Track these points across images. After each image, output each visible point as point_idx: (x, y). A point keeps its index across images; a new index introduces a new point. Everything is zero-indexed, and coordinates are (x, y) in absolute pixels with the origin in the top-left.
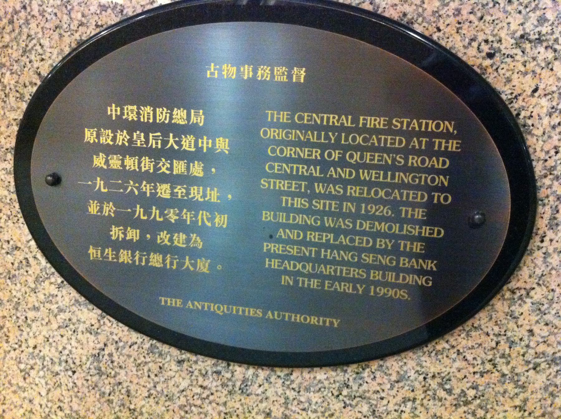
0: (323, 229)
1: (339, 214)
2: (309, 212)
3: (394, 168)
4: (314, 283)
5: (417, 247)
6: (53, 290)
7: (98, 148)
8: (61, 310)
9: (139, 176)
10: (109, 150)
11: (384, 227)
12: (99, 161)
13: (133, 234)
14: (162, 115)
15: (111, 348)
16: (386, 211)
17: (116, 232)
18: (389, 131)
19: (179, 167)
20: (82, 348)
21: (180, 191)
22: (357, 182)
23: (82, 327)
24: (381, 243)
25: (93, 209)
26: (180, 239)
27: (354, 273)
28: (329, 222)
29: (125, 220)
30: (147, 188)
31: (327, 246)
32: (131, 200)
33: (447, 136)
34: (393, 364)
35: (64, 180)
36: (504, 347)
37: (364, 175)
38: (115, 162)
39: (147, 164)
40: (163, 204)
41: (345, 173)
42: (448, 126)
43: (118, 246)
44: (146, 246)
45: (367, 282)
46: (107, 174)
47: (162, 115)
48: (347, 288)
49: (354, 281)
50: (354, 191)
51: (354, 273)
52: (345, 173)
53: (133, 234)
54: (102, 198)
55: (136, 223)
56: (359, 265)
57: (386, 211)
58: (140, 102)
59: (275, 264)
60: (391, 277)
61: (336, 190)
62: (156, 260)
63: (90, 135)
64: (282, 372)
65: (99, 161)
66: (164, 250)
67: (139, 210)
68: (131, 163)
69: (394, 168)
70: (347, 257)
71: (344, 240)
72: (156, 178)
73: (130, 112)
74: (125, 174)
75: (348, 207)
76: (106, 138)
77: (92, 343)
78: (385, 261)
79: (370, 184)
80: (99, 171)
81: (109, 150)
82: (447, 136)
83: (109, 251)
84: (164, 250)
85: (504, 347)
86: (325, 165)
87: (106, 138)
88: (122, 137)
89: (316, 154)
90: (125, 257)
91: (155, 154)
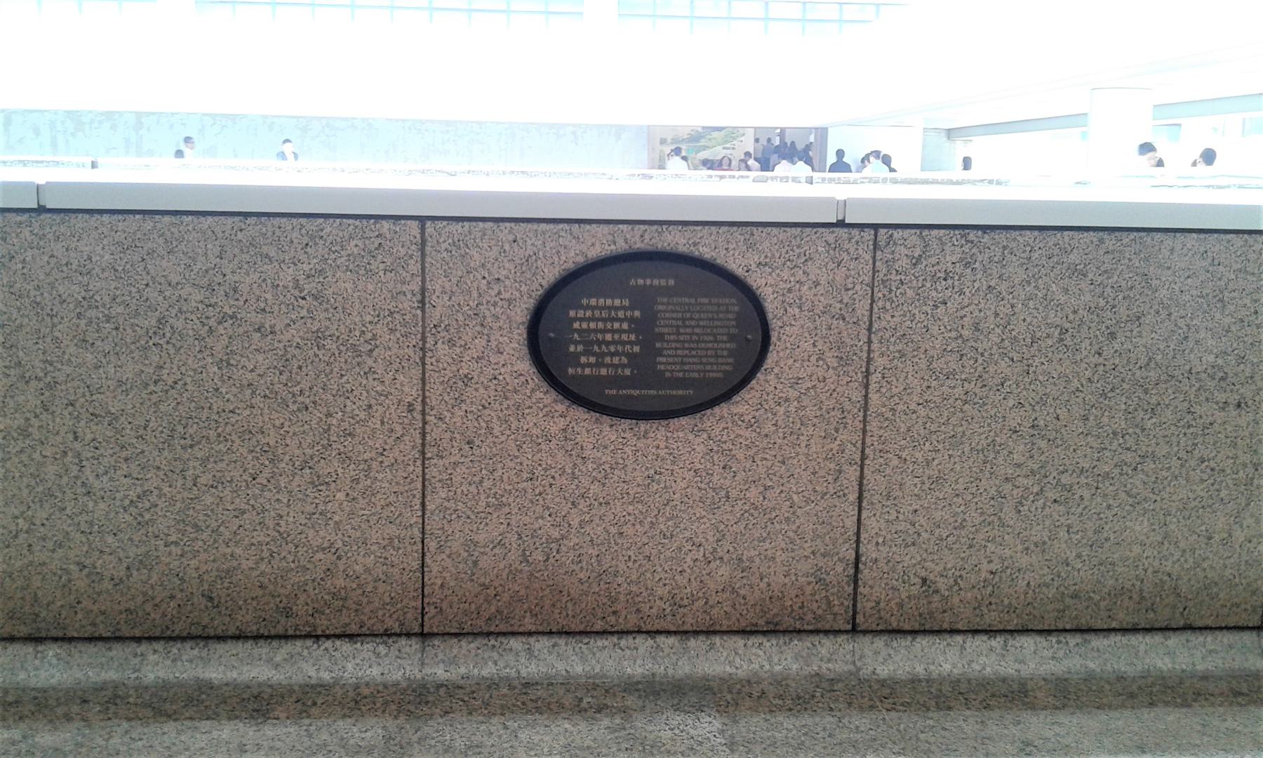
0: (684, 348)
1: (691, 341)
2: (678, 341)
3: (713, 319)
4: (681, 375)
5: (725, 353)
6: (542, 395)
7: (576, 319)
8: (545, 406)
9: (596, 331)
10: (581, 320)
11: (710, 345)
12: (576, 325)
13: (592, 360)
14: (609, 302)
15: (574, 423)
16: (711, 338)
17: (583, 360)
18: (710, 304)
19: (616, 325)
20: (556, 426)
21: (616, 337)
22: (698, 326)
23: (557, 414)
24: (709, 353)
25: (572, 349)
26: (616, 360)
27: (699, 367)
28: (687, 345)
29: (587, 353)
30: (600, 336)
31: (686, 356)
32: (591, 343)
33: (733, 305)
34: (717, 410)
35: (1136, 148)
36: (765, 396)
37: (701, 323)
38: (585, 326)
39: (601, 325)
40: (608, 344)
41: (693, 323)
42: (734, 301)
43: (583, 366)
44: (599, 365)
45: (705, 371)
46: (580, 331)
47: (609, 302)
48: (696, 375)
49: (698, 371)
50: (697, 330)
51: (699, 367)
52: (693, 323)
53: (592, 360)
54: (576, 343)
55: (594, 354)
56: (701, 363)
57: (711, 338)
58: (605, 297)
59: (662, 367)
60: (715, 367)
61: (689, 330)
62: (604, 372)
63: (572, 313)
64: (664, 422)
65: (576, 325)
66: (608, 366)
67: (596, 348)
68: (592, 325)
69: (713, 319)
70: (695, 360)
71: (694, 353)
72: (604, 331)
73: (593, 302)
74: (589, 331)
75: (695, 337)
76: (581, 314)
77: (562, 423)
78: (712, 360)
79: (704, 327)
80: (576, 330)
81: (581, 320)
82: (733, 305)
83: (579, 370)
84: (608, 366)
85: (765, 396)
86: (684, 320)
87: (581, 314)
88: (589, 313)
89: (680, 315)
90: (587, 371)
91: (604, 320)
